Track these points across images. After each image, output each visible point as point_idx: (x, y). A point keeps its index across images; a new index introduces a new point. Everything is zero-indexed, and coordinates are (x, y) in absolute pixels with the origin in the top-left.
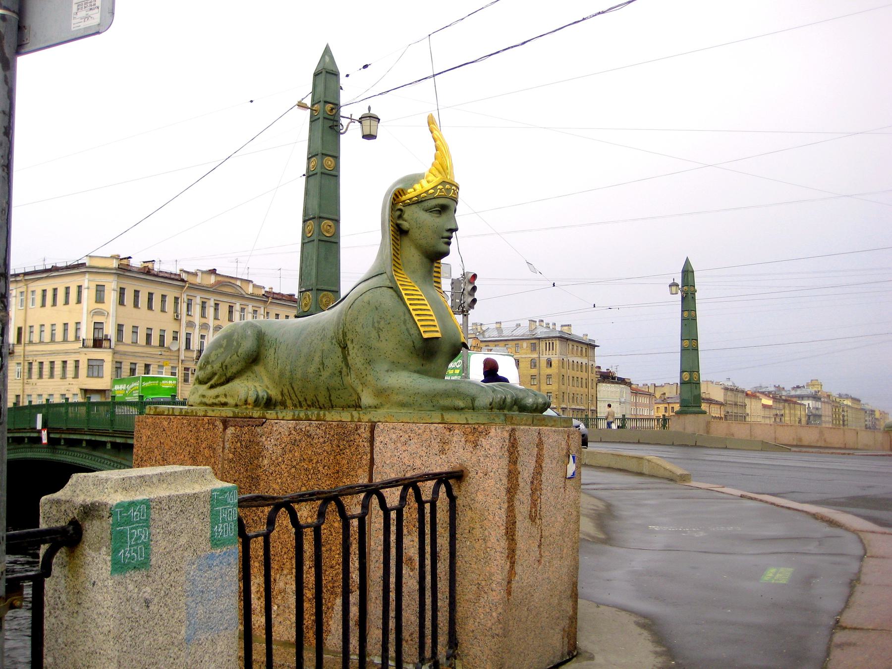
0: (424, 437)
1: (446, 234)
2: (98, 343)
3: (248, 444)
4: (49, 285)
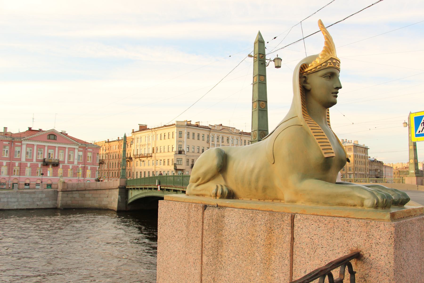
0: (329, 226)
1: (335, 91)
2: (180, 152)
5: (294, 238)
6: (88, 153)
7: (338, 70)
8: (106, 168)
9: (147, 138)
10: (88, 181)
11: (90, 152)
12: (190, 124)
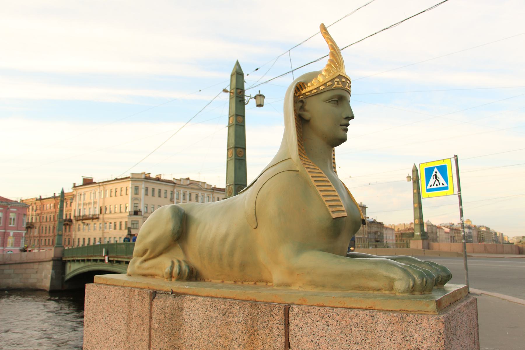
0: (344, 323)
1: (344, 122)
2: (136, 213)
5: (289, 343)
6: (11, 214)
7: (349, 92)
8: (36, 234)
9: (92, 195)
10: (9, 251)
11: (13, 212)
12: (149, 177)
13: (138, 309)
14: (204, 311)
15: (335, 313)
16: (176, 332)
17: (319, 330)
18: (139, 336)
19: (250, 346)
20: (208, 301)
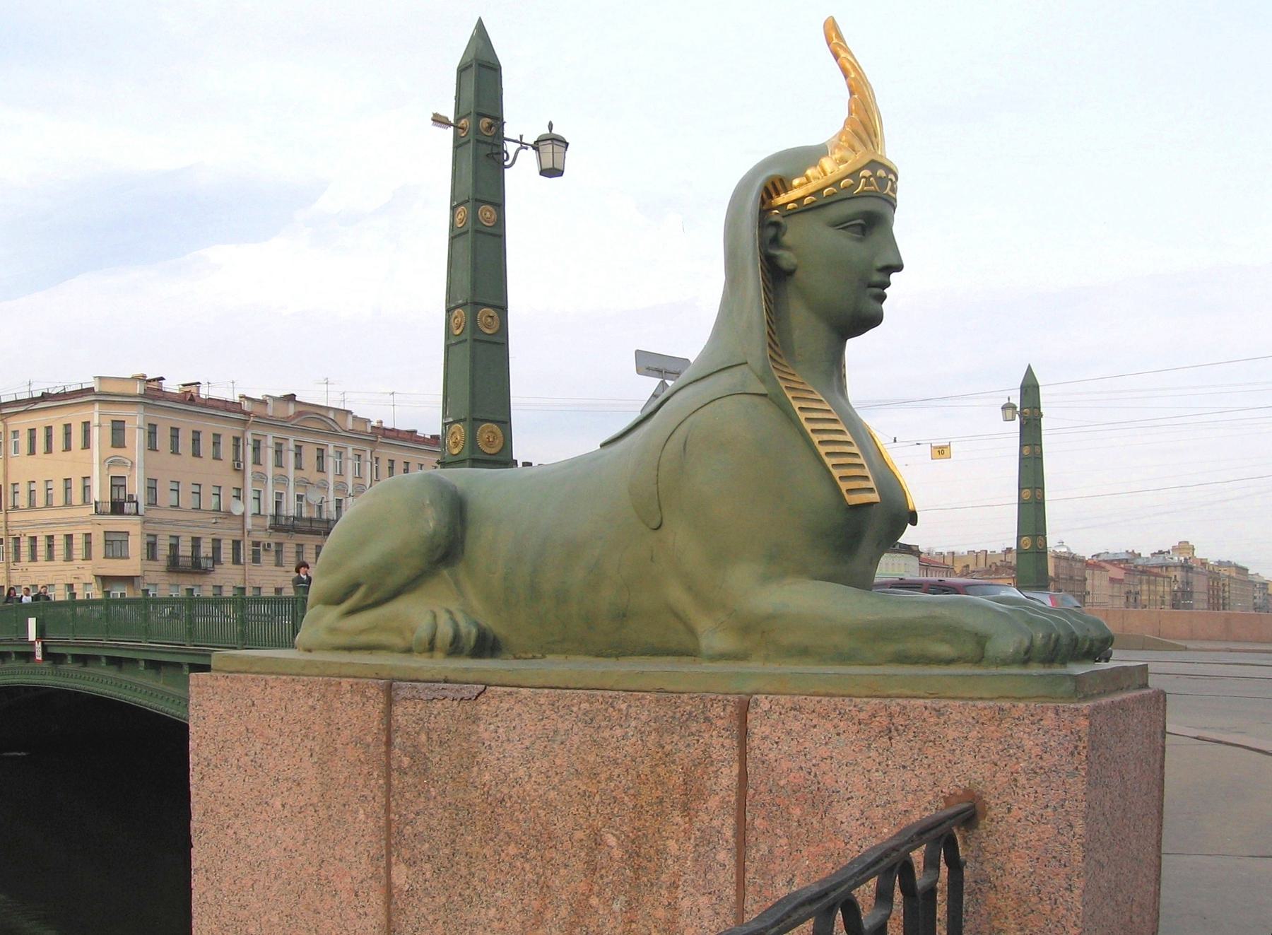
1: (877, 277)
2: (117, 508)
3: (445, 737)
4: (38, 421)
7: (892, 203)
12: (159, 390)
13: (350, 726)
14: (536, 720)
15: (855, 706)
16: (460, 772)
17: (818, 745)
18: (357, 789)
19: (655, 789)
20: (544, 696)
